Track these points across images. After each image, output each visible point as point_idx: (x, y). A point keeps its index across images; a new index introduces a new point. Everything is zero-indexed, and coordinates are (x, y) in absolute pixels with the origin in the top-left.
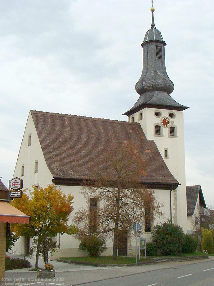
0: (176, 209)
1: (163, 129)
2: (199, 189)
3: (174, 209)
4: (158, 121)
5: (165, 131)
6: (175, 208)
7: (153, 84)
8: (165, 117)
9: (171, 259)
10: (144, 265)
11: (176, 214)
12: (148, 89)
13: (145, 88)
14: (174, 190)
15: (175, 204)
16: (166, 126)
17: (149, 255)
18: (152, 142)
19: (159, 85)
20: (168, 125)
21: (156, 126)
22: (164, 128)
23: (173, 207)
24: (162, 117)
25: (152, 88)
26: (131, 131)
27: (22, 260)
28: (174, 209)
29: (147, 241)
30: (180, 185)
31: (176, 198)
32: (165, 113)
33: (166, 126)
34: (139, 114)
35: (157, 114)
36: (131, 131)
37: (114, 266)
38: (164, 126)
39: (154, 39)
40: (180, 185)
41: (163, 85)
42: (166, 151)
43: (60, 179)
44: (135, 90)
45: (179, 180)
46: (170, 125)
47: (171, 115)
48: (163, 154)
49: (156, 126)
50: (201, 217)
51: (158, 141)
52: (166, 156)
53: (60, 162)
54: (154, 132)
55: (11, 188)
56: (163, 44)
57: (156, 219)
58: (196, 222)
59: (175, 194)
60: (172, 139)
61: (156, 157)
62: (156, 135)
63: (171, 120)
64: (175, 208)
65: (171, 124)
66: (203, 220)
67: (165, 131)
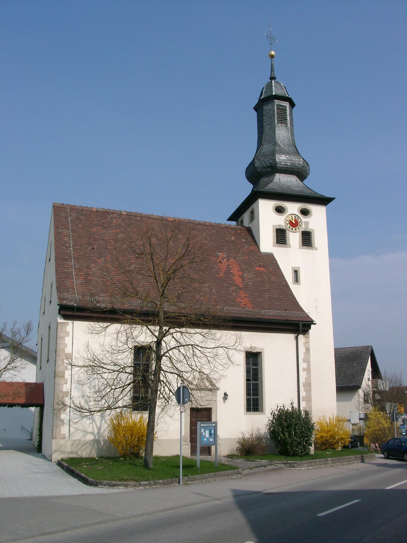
0: (308, 370)
1: (289, 234)
2: (370, 351)
3: (304, 369)
4: (280, 221)
5: (294, 238)
7: (271, 161)
8: (293, 214)
9: (290, 464)
10: (206, 481)
11: (308, 378)
12: (264, 171)
13: (259, 170)
14: (304, 335)
15: (307, 361)
16: (296, 229)
18: (270, 258)
19: (283, 163)
20: (299, 228)
21: (276, 229)
22: (291, 233)
23: (302, 365)
25: (270, 169)
26: (233, 238)
28: (304, 369)
29: (260, 432)
30: (315, 324)
31: (308, 350)
32: (293, 208)
33: (296, 229)
34: (249, 213)
35: (280, 210)
36: (233, 238)
37: (114, 485)
38: (292, 229)
39: (274, 94)
40: (315, 324)
41: (288, 164)
43: (71, 308)
45: (312, 316)
46: (303, 228)
47: (305, 212)
48: (289, 277)
49: (276, 229)
50: (374, 393)
52: (297, 280)
53: (84, 282)
54: (274, 240)
58: (366, 401)
59: (307, 343)
60: (306, 251)
61: (273, 279)
63: (303, 219)
65: (303, 226)
66: (378, 397)
67: (294, 238)
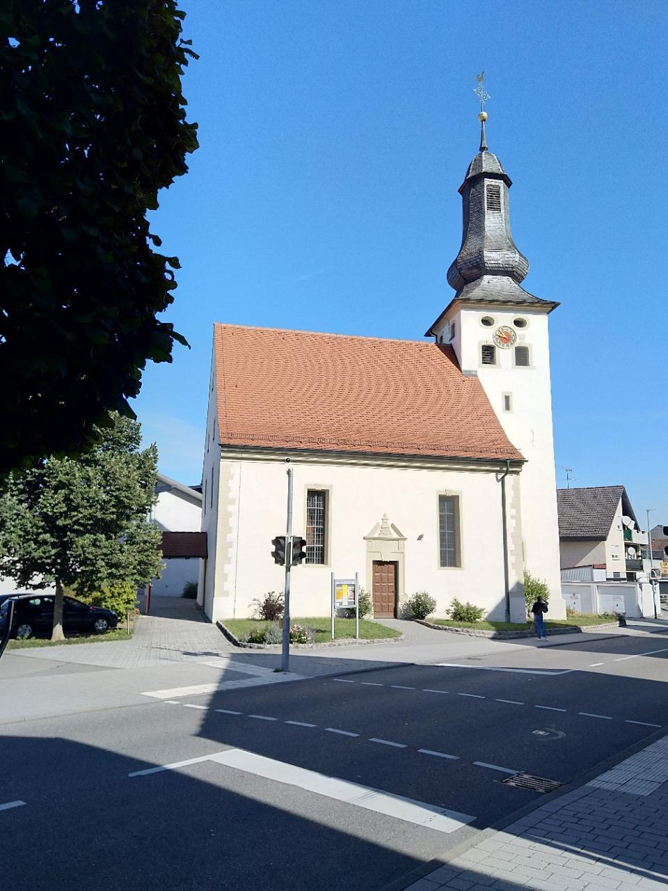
2: (620, 491)
4: (487, 336)
5: (505, 355)
6: (515, 514)
17: (353, 609)
18: (472, 375)
24: (498, 326)
27: (105, 427)
32: (504, 319)
42: (507, 398)
44: (450, 287)
47: (519, 323)
48: (497, 405)
51: (486, 375)
55: (503, 477)
56: (502, 181)
57: (157, 504)
62: (511, 408)
64: (515, 514)
65: (518, 340)
